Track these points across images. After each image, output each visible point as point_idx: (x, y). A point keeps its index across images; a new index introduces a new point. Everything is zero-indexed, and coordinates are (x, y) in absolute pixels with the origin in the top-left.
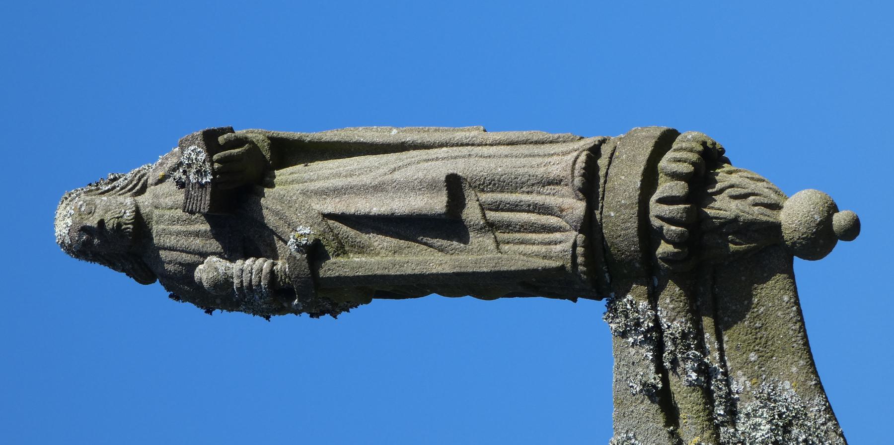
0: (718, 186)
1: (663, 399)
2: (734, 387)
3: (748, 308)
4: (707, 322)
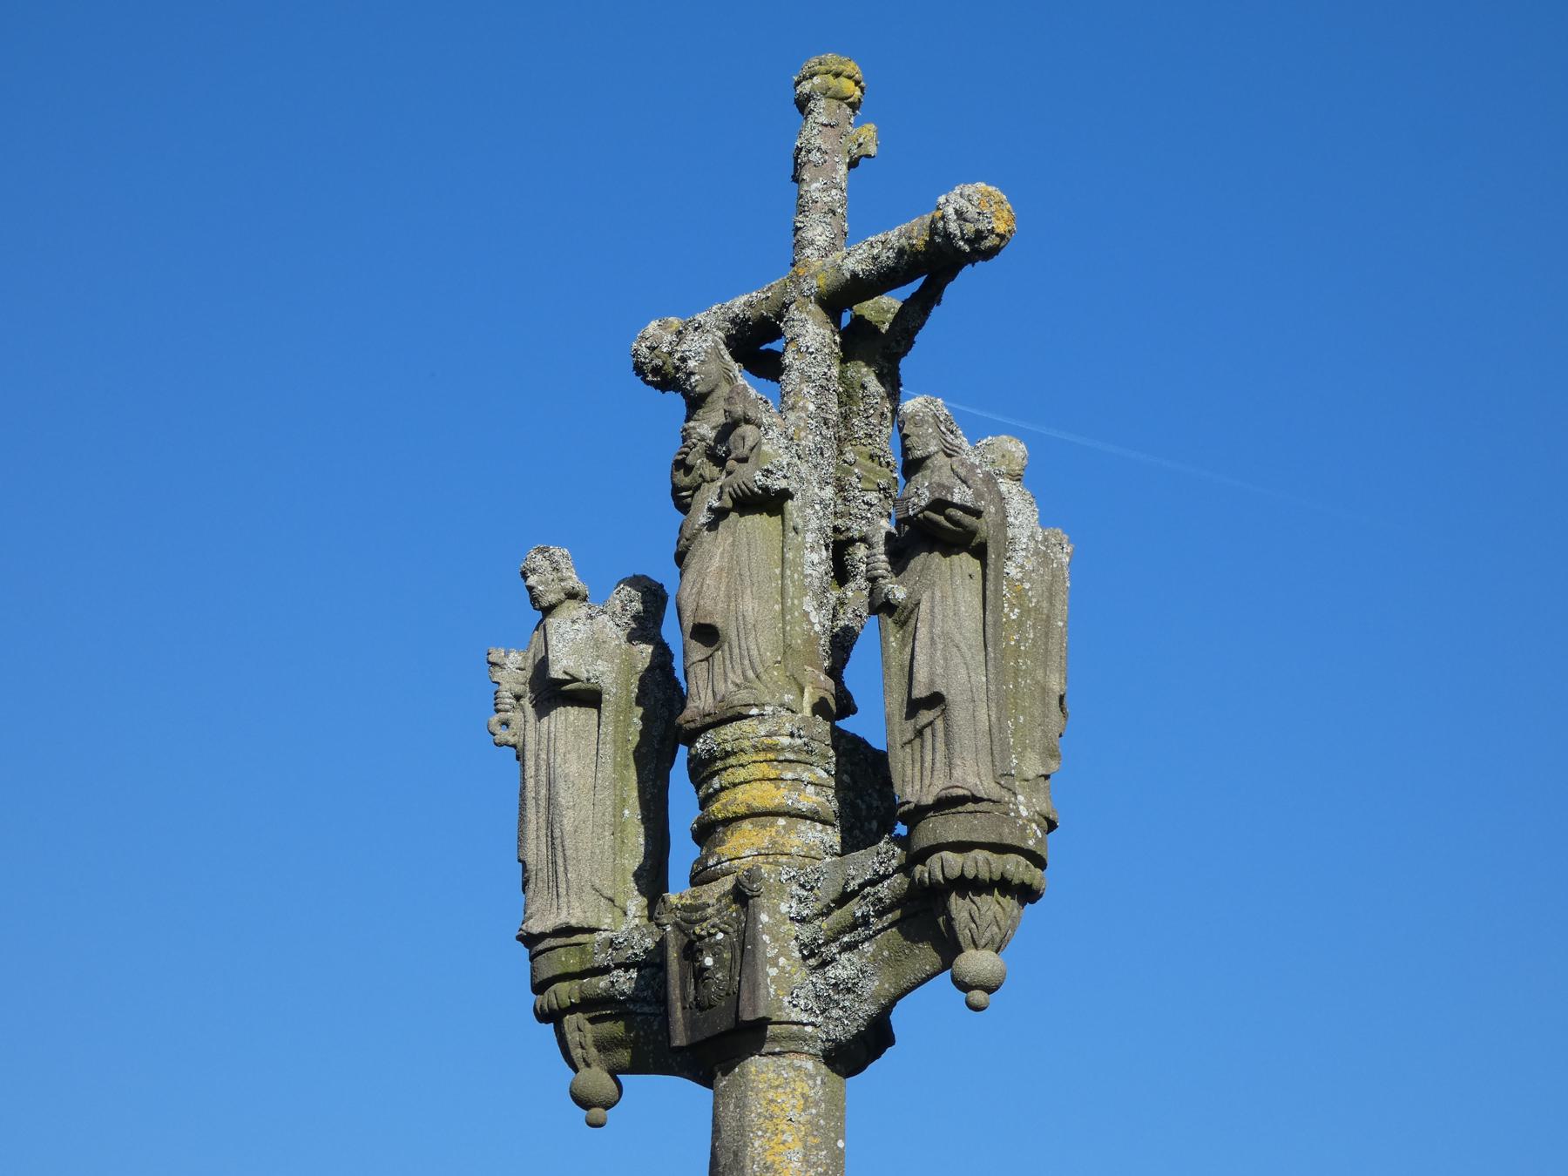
0: (976, 899)
1: (844, 898)
2: (866, 944)
3: (914, 942)
4: (898, 913)
